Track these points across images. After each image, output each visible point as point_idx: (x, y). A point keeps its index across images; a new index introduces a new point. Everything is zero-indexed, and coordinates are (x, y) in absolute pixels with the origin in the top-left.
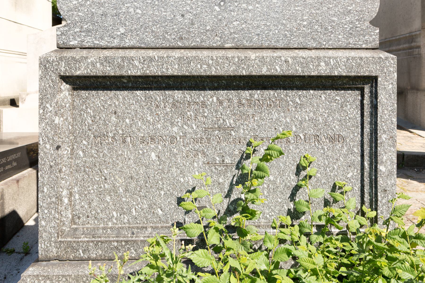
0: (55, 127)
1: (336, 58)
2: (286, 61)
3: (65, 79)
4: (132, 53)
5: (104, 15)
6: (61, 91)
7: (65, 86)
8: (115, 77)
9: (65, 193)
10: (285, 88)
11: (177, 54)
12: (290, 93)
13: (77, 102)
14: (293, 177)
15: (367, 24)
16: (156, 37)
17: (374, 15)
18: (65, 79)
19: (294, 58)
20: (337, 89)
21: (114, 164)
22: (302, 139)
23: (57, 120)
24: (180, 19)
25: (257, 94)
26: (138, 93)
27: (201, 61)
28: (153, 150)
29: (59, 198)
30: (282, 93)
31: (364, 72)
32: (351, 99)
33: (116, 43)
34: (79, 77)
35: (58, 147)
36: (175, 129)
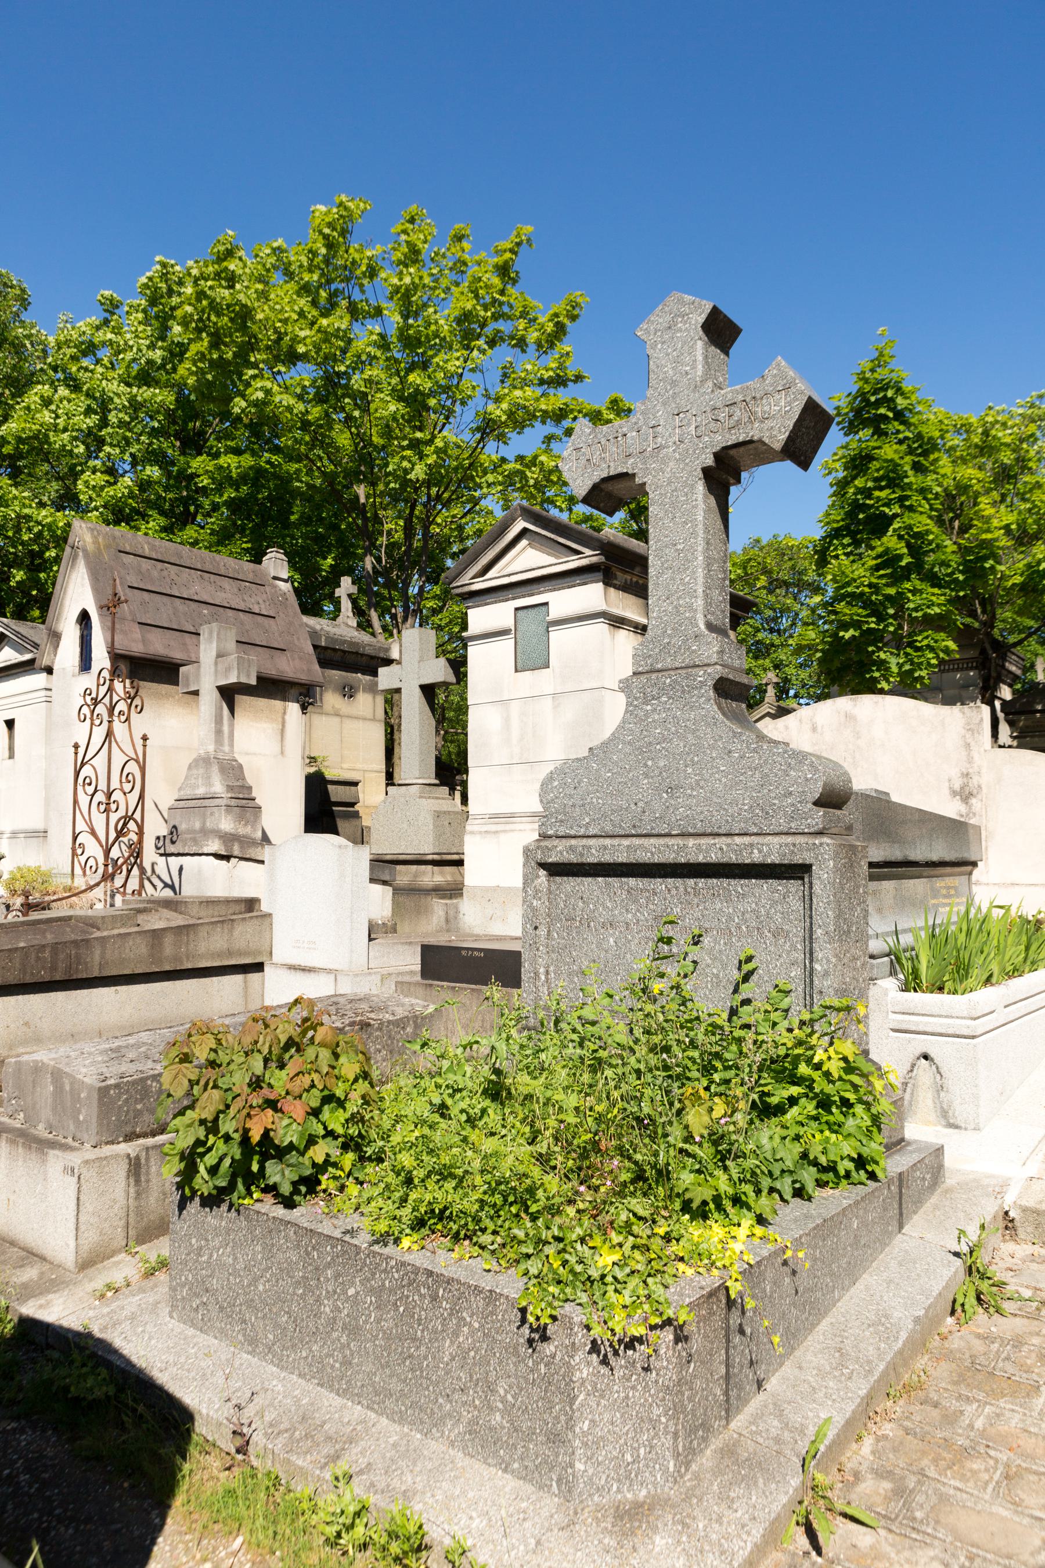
0: (534, 910)
1: (768, 845)
2: (721, 849)
3: (543, 865)
4: (592, 842)
5: (574, 806)
6: (538, 876)
7: (542, 873)
8: (577, 864)
9: (542, 970)
10: (727, 877)
11: (626, 842)
12: (733, 882)
13: (553, 887)
14: (735, 971)
15: (810, 806)
16: (614, 826)
17: (817, 796)
18: (543, 865)
19: (728, 845)
20: (779, 878)
21: (581, 948)
22: (141, 918)
23: (535, 903)
24: (633, 807)
25: (701, 882)
26: (600, 879)
27: (646, 850)
28: (612, 935)
29: (536, 974)
30: (725, 882)
31: (798, 859)
32: (793, 890)
33: (582, 832)
34: (552, 864)
35: (536, 928)
36: (630, 916)
